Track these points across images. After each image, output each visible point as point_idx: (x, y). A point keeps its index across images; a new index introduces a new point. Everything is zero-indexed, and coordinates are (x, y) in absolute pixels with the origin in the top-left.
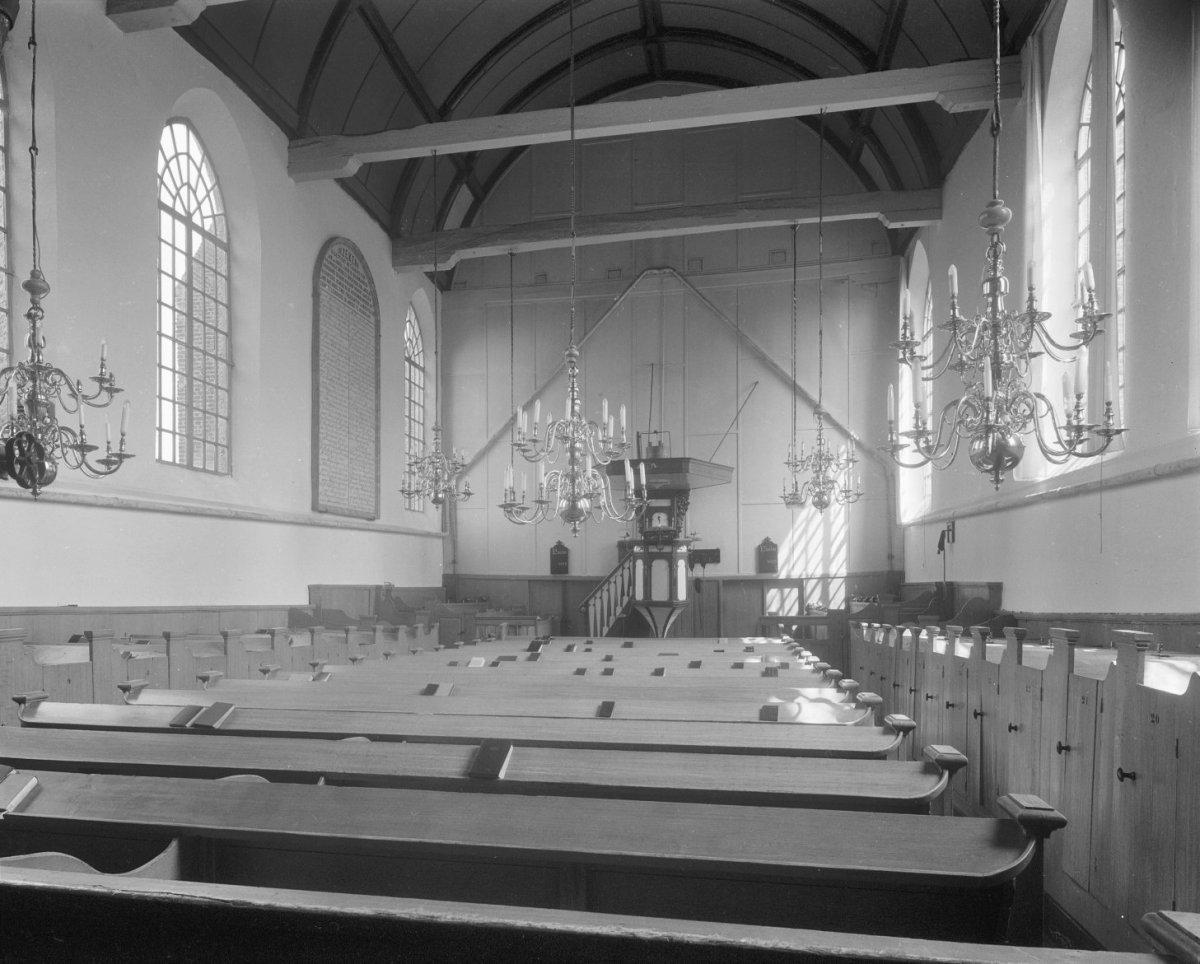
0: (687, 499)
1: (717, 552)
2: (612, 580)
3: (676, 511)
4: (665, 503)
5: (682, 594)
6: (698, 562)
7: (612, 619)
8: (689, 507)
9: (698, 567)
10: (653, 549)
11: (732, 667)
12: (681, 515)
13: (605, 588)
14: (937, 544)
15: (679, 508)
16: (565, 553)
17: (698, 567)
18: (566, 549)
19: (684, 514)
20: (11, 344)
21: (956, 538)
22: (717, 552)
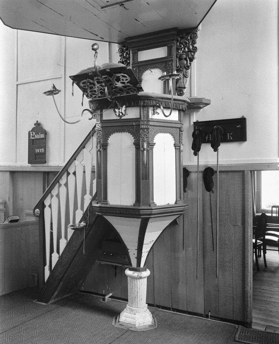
0: (194, 43)
1: (242, 121)
2: (71, 170)
3: (176, 63)
4: (160, 53)
5: (165, 191)
6: (205, 142)
7: (63, 244)
8: (196, 55)
9: (206, 149)
10: (109, 115)
11: (38, 128)
12: (184, 68)
13: (63, 181)
14: (159, 77)
15: (180, 59)
16: (42, 136)
17: (206, 149)
18: (45, 133)
19: (188, 67)
20: (217, 164)
21: (18, 80)
22: (242, 121)
